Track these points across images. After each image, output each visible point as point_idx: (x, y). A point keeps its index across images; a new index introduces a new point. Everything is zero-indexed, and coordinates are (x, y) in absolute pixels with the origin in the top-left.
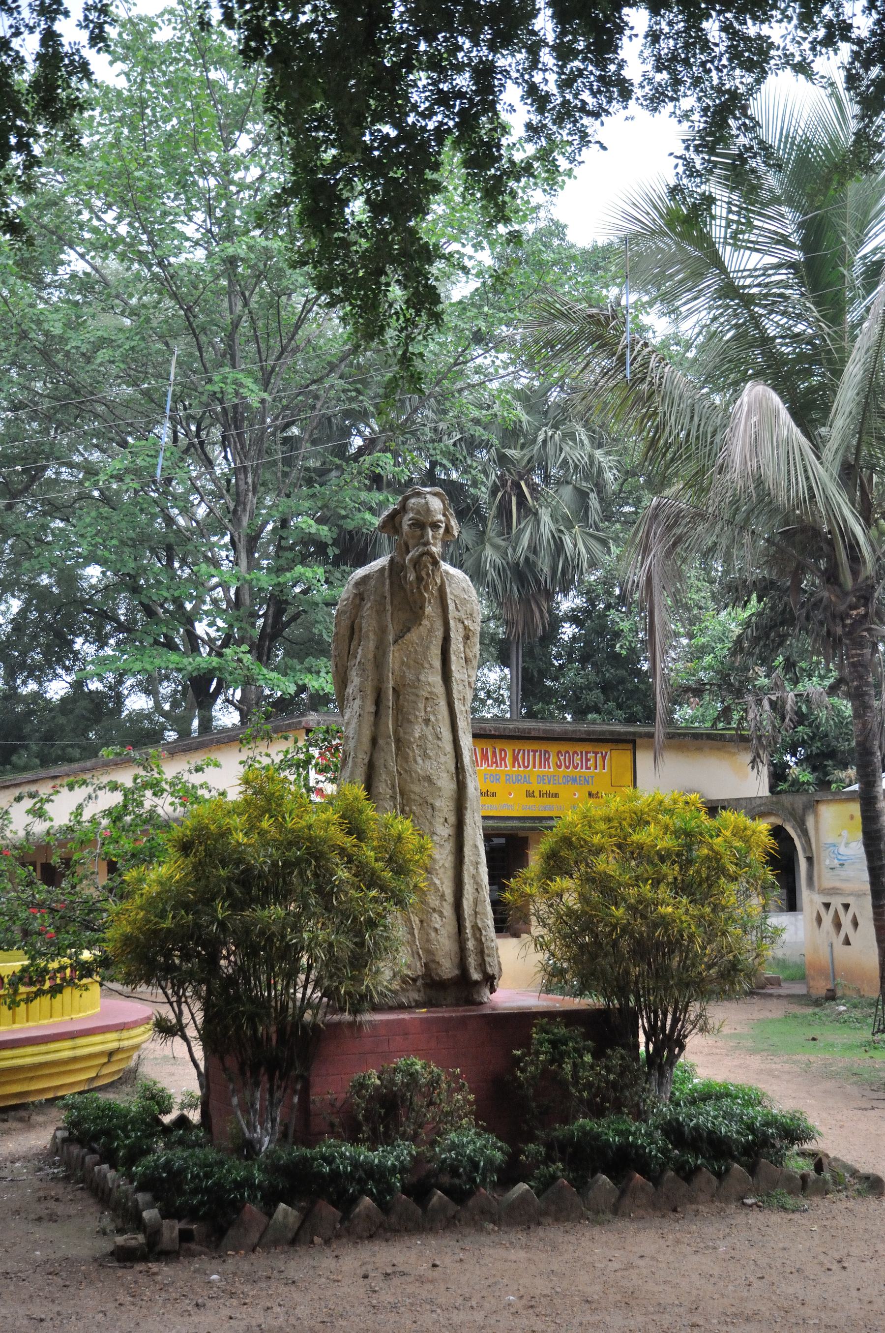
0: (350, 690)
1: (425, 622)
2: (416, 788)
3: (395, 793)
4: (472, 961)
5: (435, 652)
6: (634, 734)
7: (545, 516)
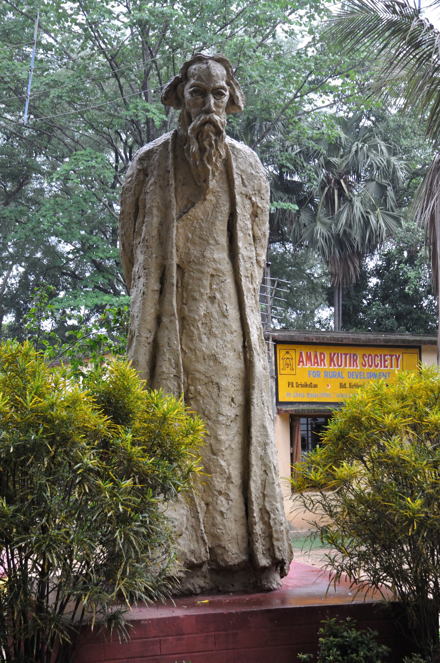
0: (135, 269)
1: (210, 197)
2: (201, 367)
3: (179, 372)
4: (260, 546)
5: (221, 227)
6: (420, 341)
7: (357, 203)
